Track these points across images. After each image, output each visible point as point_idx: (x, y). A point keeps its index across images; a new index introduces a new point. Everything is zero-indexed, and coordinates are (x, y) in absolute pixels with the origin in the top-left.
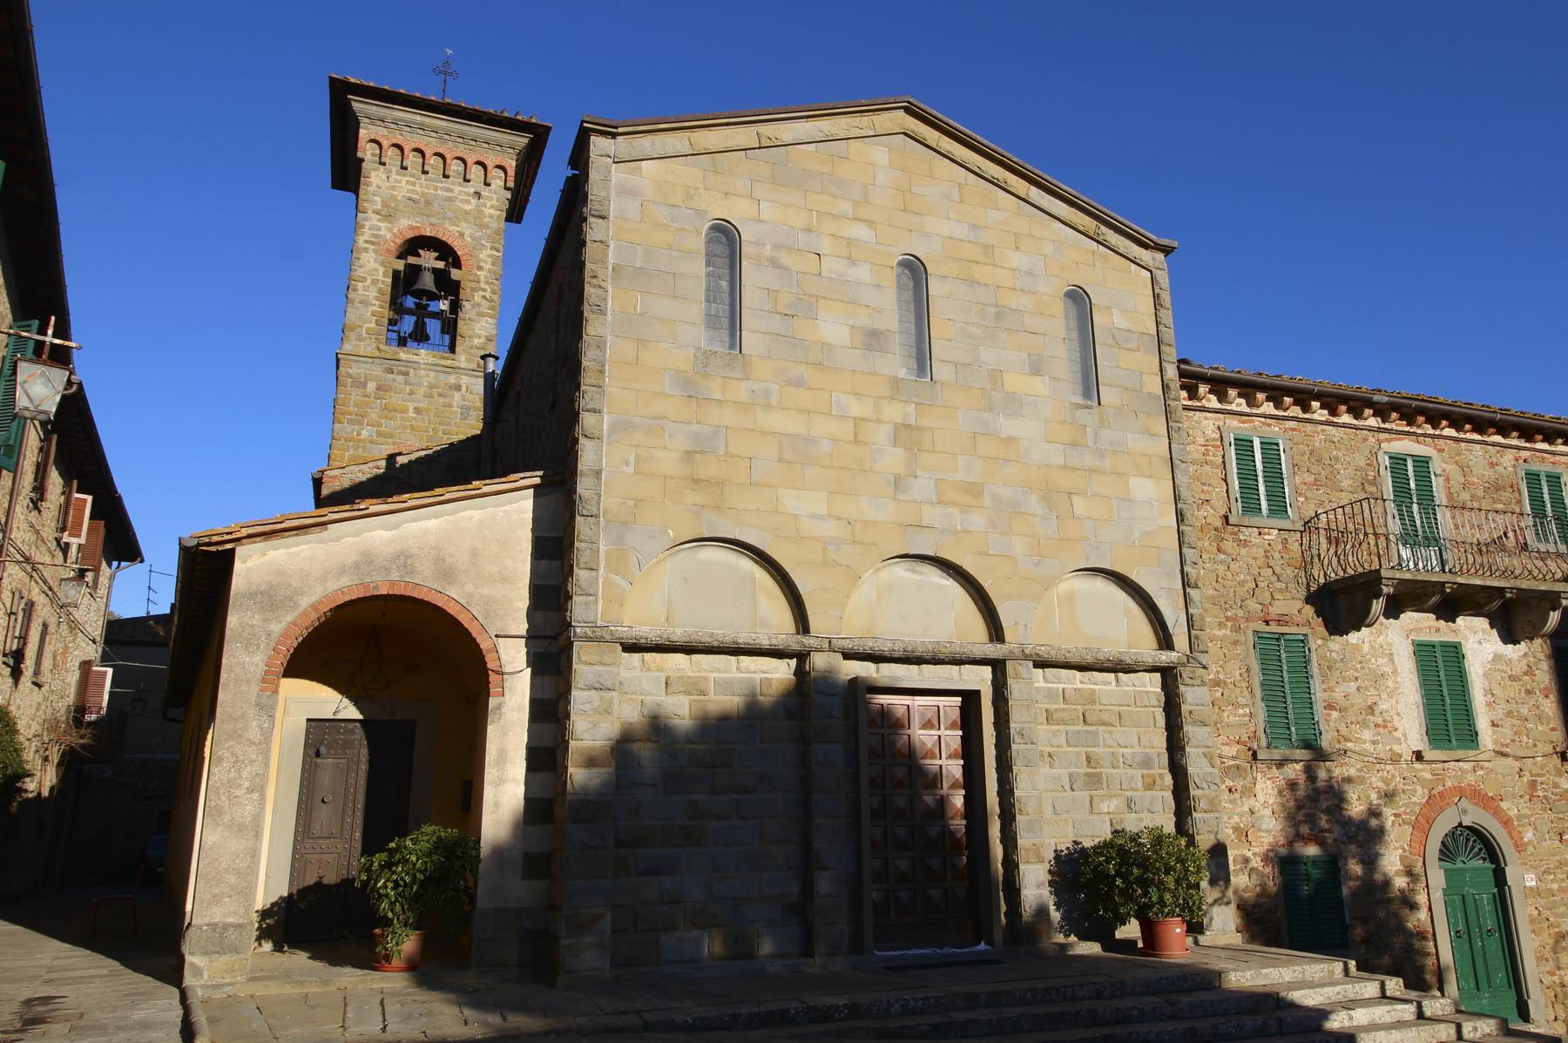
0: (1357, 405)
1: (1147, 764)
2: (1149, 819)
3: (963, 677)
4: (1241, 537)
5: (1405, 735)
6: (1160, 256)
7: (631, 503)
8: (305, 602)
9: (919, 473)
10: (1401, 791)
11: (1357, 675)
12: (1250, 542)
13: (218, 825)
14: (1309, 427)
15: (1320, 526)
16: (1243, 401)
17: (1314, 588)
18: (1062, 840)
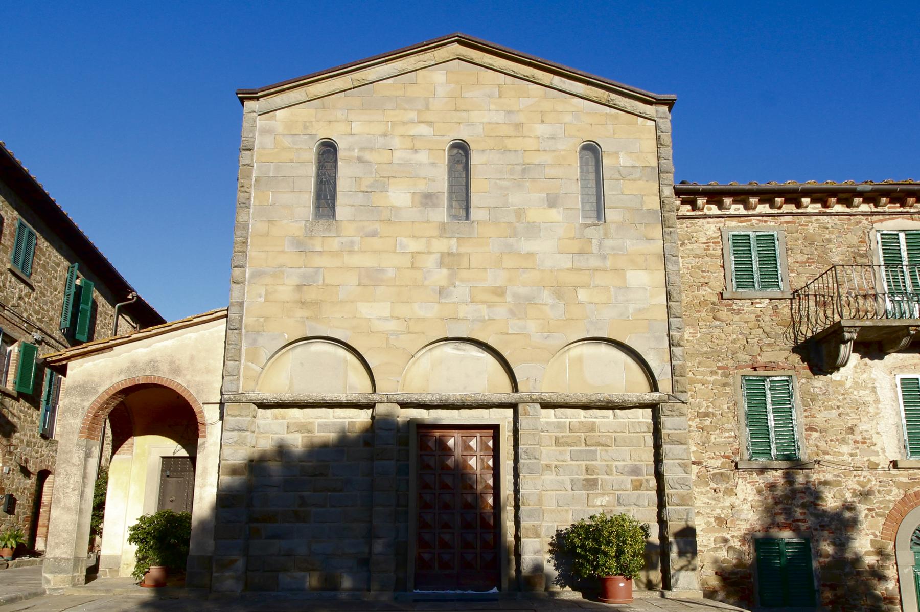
0: (846, 196)
1: (636, 472)
2: (635, 510)
3: (491, 416)
4: (735, 307)
5: (883, 450)
6: (666, 108)
7: (262, 320)
8: (101, 390)
9: (457, 284)
10: (876, 492)
11: (839, 404)
12: (743, 310)
13: (58, 507)
14: (804, 219)
15: (810, 293)
16: (741, 206)
17: (801, 340)
18: (562, 523)
